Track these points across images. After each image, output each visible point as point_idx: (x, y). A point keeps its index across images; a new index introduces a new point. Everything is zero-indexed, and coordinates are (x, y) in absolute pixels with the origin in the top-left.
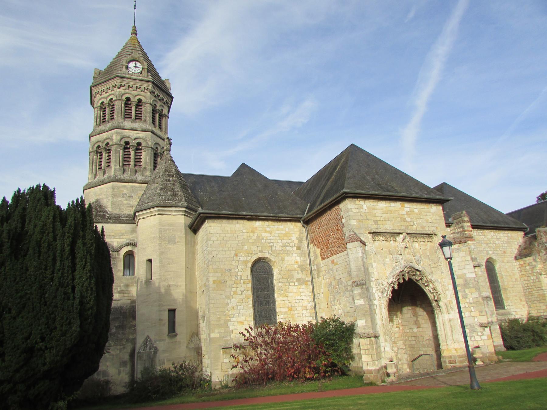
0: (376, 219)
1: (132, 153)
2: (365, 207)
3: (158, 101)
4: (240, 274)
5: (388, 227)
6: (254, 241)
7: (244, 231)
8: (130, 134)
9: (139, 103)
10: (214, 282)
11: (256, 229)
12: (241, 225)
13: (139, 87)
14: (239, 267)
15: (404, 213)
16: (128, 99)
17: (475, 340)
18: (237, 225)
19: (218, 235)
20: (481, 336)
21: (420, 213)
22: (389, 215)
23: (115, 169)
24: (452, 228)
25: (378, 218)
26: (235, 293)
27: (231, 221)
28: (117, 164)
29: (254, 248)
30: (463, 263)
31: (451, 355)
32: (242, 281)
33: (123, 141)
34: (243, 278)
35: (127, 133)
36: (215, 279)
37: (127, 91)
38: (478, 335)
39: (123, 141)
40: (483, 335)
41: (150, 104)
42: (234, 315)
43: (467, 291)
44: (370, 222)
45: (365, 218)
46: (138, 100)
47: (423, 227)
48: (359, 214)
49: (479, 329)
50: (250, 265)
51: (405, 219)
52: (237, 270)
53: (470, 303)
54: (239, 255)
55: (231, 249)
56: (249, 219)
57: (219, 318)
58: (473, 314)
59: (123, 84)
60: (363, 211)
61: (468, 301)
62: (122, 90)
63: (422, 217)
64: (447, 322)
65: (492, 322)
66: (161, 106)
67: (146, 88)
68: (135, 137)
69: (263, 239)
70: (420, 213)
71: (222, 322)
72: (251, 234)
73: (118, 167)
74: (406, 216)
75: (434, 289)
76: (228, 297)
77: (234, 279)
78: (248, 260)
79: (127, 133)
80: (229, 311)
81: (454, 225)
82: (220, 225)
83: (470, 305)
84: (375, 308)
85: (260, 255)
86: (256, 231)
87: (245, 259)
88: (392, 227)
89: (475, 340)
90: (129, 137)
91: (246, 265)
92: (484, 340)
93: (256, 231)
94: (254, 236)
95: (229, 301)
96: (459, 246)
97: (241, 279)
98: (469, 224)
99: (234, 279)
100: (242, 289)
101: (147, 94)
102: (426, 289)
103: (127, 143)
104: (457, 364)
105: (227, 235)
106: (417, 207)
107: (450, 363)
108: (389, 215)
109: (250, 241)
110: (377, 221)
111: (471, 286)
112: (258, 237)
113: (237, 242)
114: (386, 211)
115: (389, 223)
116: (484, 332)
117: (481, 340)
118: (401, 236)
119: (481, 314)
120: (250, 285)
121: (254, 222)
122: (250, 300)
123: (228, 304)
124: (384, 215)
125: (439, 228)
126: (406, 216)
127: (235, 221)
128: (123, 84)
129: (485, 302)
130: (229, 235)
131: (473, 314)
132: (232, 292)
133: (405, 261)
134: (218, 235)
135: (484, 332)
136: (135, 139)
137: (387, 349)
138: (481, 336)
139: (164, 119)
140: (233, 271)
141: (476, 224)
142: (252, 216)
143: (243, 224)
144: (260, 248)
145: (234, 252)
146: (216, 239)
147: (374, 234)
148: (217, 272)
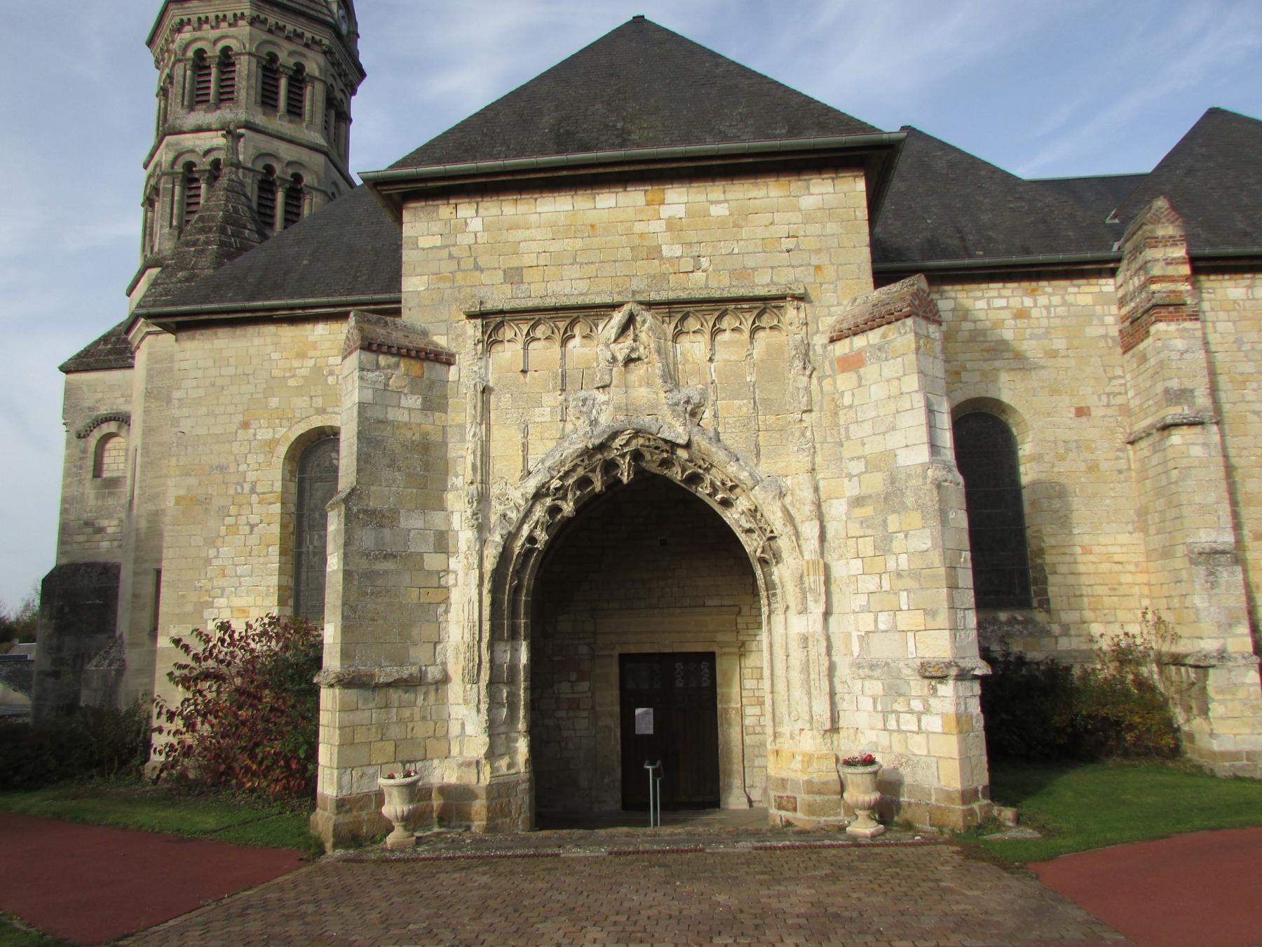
0: (515, 262)
1: (280, 197)
2: (476, 224)
3: (305, 51)
4: (251, 476)
5: (570, 287)
6: (301, 382)
7: (275, 356)
8: (198, 142)
9: (227, 60)
10: (178, 500)
11: (314, 346)
12: (269, 340)
13: (221, 15)
14: (251, 459)
15: (658, 226)
16: (200, 53)
17: (899, 731)
18: (257, 341)
19: (200, 374)
20: (919, 715)
21: (741, 217)
22: (579, 244)
23: (161, 235)
24: (1120, 278)
25: (529, 260)
26: (233, 529)
27: (239, 331)
28: (167, 224)
29: (301, 402)
30: (892, 407)
31: (784, 774)
32: (255, 498)
33: (181, 161)
34: (259, 489)
35: (188, 141)
36: (182, 492)
37: (198, 34)
38: (911, 712)
39: (181, 161)
40: (927, 710)
41: (250, 54)
42: (223, 589)
43: (893, 522)
44: (485, 278)
45: (468, 264)
46: (295, 64)
47: (742, 273)
48: (446, 252)
49: (918, 687)
50: (282, 450)
51: (658, 249)
52: (243, 467)
53: (899, 575)
54: (254, 424)
55: (231, 409)
56: (293, 320)
57: (183, 596)
58: (904, 620)
59: (185, 18)
60: (465, 239)
61: (891, 565)
62: (186, 35)
63: (745, 232)
64: (794, 646)
65: (1222, 656)
66: (291, 54)
67: (239, 12)
68: (208, 147)
69: (331, 373)
70: (741, 217)
71: (189, 608)
72: (296, 363)
73: (167, 230)
74: (663, 238)
75: (754, 512)
76: (211, 542)
77: (232, 492)
78: (277, 436)
79: (188, 141)
80: (211, 579)
81: (1124, 265)
82: (208, 345)
83: (900, 584)
84: (451, 581)
85: (317, 422)
86: (311, 353)
87: (270, 436)
88: (583, 286)
89: (899, 731)
90: (192, 151)
91: (272, 452)
92: (928, 733)
93: (311, 353)
94: (304, 368)
95: (212, 552)
96: (884, 336)
97: (253, 490)
98: (1180, 252)
99: (232, 492)
100: (254, 519)
101: (244, 28)
102: (734, 518)
103: (190, 166)
104: (799, 815)
105: (225, 371)
106: (730, 196)
107: (780, 807)
108: (579, 244)
109: (292, 382)
110: (519, 270)
111: (910, 500)
112: (317, 369)
113: (251, 388)
114: (558, 231)
115: (574, 272)
116: (932, 701)
117: (920, 731)
118: (618, 317)
119: (931, 624)
120: (277, 508)
121: (308, 327)
122: (275, 550)
123: (208, 561)
124: (556, 246)
125: (830, 272)
126: (663, 238)
127: (252, 330)
128: (185, 18)
129: (1202, 570)
130: (232, 371)
131: (904, 620)
132: (223, 529)
133: (618, 409)
134: (200, 374)
135: (932, 701)
136: (289, 164)
137: (470, 729)
138: (919, 715)
139: (309, 89)
140: (232, 469)
141: (1207, 251)
142: (292, 308)
143: (276, 335)
144: (319, 402)
145: (238, 418)
146: (194, 383)
147: (492, 321)
148: (188, 475)
